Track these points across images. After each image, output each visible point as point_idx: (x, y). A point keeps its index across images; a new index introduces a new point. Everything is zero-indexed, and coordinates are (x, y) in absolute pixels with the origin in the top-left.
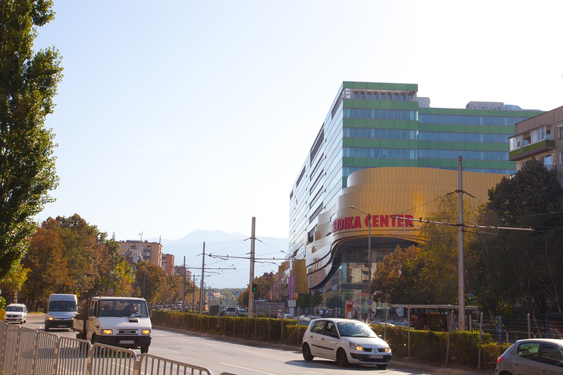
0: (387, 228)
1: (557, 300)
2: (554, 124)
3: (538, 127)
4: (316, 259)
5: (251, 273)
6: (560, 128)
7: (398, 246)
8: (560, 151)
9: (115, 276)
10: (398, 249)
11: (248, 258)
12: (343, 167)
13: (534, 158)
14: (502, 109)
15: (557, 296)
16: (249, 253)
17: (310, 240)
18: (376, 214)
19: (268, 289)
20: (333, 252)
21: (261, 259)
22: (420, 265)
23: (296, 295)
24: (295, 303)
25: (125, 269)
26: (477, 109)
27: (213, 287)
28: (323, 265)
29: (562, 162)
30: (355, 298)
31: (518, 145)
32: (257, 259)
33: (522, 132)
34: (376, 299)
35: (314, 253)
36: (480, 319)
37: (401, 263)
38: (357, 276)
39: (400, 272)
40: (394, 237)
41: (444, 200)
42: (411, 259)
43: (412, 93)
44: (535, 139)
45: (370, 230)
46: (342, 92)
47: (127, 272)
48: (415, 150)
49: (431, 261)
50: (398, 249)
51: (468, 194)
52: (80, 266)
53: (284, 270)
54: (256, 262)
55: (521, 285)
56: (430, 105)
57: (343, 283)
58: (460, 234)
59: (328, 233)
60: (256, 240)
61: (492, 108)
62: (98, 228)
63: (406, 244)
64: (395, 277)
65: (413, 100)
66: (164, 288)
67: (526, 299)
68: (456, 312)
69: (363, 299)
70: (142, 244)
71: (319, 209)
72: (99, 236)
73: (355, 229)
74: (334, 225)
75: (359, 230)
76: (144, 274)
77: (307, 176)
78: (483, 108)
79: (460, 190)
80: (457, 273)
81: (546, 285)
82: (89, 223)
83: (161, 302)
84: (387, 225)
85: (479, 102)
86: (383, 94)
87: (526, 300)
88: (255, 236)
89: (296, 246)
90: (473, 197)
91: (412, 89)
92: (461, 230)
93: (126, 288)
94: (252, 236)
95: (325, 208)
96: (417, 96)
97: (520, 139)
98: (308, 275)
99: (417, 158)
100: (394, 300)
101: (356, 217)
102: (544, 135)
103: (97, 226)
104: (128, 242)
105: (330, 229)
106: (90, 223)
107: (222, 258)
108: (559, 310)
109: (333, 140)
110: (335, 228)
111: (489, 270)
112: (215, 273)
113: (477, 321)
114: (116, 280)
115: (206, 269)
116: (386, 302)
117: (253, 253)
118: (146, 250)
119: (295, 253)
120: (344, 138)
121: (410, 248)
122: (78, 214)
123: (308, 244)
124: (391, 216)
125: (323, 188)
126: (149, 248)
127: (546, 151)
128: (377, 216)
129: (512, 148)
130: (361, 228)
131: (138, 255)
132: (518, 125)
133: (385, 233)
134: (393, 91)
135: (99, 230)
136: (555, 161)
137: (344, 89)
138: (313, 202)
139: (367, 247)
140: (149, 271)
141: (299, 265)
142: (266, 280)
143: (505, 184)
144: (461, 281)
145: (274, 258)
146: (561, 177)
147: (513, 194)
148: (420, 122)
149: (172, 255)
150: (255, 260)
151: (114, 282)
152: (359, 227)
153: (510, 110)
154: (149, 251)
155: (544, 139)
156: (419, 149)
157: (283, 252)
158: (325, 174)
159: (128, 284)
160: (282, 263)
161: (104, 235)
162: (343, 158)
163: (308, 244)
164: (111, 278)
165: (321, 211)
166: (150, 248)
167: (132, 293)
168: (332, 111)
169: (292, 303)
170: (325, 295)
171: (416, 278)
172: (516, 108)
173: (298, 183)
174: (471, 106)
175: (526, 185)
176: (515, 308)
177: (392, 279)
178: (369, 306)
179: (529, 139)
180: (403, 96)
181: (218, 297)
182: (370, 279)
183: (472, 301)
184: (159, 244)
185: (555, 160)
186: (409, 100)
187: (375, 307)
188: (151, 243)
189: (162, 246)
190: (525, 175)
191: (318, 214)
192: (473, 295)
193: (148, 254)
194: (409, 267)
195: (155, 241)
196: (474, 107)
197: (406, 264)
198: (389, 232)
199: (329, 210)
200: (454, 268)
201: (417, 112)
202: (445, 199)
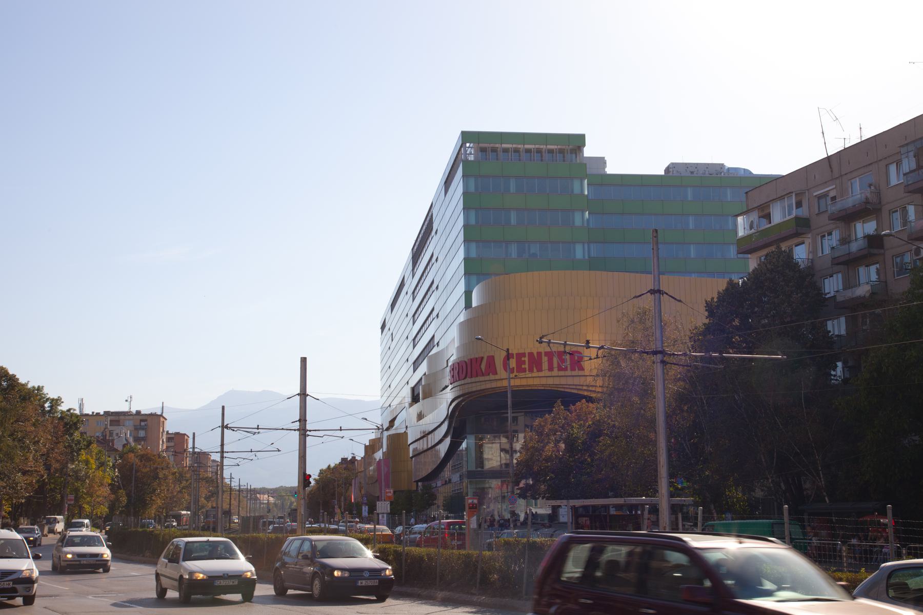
0: (541, 374)
1: (823, 483)
2: (808, 190)
3: (782, 196)
4: (424, 432)
5: (301, 455)
6: (818, 197)
7: (559, 401)
8: (818, 235)
9: (76, 472)
10: (559, 407)
11: (295, 430)
12: (465, 274)
13: (779, 247)
14: (723, 174)
15: (822, 476)
16: (296, 421)
17: (415, 399)
18: (521, 351)
19: (348, 485)
20: (450, 417)
21: (319, 430)
22: (595, 433)
23: (390, 492)
24: (389, 506)
25: (98, 459)
26: (682, 175)
27: (256, 485)
28: (437, 441)
29: (822, 253)
30: (491, 494)
31: (751, 227)
32: (310, 431)
33: (756, 205)
34: (523, 495)
35: (421, 421)
36: (696, 518)
37: (564, 430)
38: (493, 456)
39: (563, 446)
40: (553, 389)
41: (633, 321)
42: (579, 423)
43: (576, 150)
44: (777, 217)
45: (510, 378)
46: (460, 150)
47: (102, 465)
48: (583, 243)
49: (614, 426)
50: (559, 407)
51: (671, 296)
52: (9, 458)
53: (374, 453)
54: (308, 435)
55: (763, 460)
56: (606, 170)
57: (468, 470)
58: (658, 369)
59: (443, 386)
60: (308, 398)
61: (707, 172)
62: (45, 391)
63: (570, 399)
64: (554, 456)
65: (578, 161)
66: (168, 490)
67: (771, 482)
68: (655, 510)
69: (503, 495)
70: (131, 417)
71: (428, 347)
72: (47, 405)
73: (487, 378)
74: (452, 372)
75: (493, 379)
76: (133, 468)
77: (407, 293)
78: (692, 173)
79: (656, 289)
80: (654, 443)
81: (804, 458)
82: (28, 382)
83: (165, 514)
84: (540, 369)
85: (686, 164)
86: (528, 151)
87: (771, 485)
88: (306, 390)
89: (393, 410)
90: (680, 301)
91: (577, 142)
92: (659, 361)
93: (99, 493)
94: (300, 391)
95: (438, 346)
96: (585, 156)
97: (754, 216)
98: (412, 458)
99: (587, 257)
100: (554, 494)
101: (489, 357)
102: (793, 210)
103: (43, 387)
104: (107, 413)
105: (447, 379)
106: (29, 383)
107: (247, 430)
108: (827, 499)
109: (448, 230)
110: (453, 376)
111: (709, 437)
112: (244, 459)
113: (692, 524)
114: (78, 479)
115: (227, 452)
116: (541, 498)
117: (303, 420)
118: (139, 427)
119: (392, 422)
120: (466, 227)
121: (578, 404)
122: (4, 367)
123: (411, 405)
125: (433, 312)
126: (143, 424)
127: (797, 235)
128: (523, 355)
129: (741, 233)
130: (496, 376)
131: (125, 434)
132: (749, 193)
133: (536, 382)
134: (545, 146)
135: (47, 394)
136: (811, 252)
137: (464, 145)
138: (418, 336)
139: (506, 407)
140: (141, 461)
141: (398, 441)
142: (345, 470)
143: (733, 291)
144: (662, 453)
145: (341, 427)
146: (821, 278)
147: (746, 307)
148: (591, 198)
149: (185, 434)
150: (308, 433)
151: (76, 484)
152: (493, 374)
153: (735, 175)
154: (142, 428)
155: (793, 216)
156: (589, 242)
157: (366, 419)
158: (437, 288)
159: (102, 484)
160: (370, 440)
161: (56, 402)
162: (465, 259)
163: (411, 405)
164: (70, 476)
165: (431, 350)
166: (146, 423)
167: (110, 500)
168: (445, 182)
169: (383, 507)
170: (443, 492)
171: (590, 456)
172: (744, 172)
173: (393, 305)
174: (673, 171)
175: (766, 292)
176: (753, 499)
177: (548, 459)
178: (511, 506)
179: (768, 217)
180: (561, 155)
181: (264, 502)
182: (512, 460)
183: (683, 491)
184: (161, 415)
185: (810, 250)
186: (571, 161)
187: (522, 508)
188: (146, 415)
189: (166, 419)
190: (765, 274)
191: (428, 355)
192: (684, 481)
193: (142, 434)
194: (576, 437)
195: (153, 412)
196: (678, 172)
197: (572, 432)
198: (544, 381)
199: (444, 349)
200: (652, 436)
201: (586, 181)
202: (635, 318)
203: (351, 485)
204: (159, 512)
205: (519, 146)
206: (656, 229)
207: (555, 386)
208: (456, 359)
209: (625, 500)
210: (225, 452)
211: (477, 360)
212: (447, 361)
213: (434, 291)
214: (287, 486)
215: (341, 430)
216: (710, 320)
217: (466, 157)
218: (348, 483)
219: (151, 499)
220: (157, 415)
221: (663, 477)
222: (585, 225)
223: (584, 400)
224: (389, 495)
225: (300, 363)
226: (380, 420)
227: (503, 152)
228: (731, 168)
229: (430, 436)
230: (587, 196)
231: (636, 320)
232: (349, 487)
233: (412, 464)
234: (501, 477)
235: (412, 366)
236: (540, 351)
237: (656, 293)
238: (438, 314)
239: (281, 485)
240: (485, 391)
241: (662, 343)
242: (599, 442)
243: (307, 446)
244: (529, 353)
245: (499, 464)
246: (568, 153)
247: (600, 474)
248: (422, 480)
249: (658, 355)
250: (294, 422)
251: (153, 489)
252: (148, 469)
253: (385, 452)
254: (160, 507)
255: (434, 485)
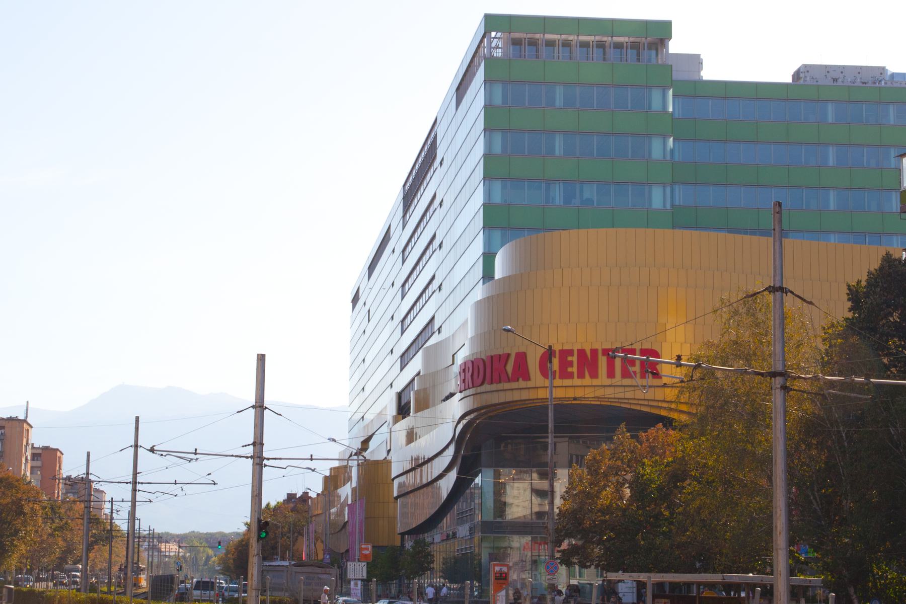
0: (595, 382)
4: (417, 459)
5: (255, 494)
7: (623, 425)
10: (622, 435)
11: (247, 457)
14: (883, 82)
16: (249, 445)
17: (403, 410)
20: (459, 441)
21: (281, 459)
24: (365, 569)
30: (514, 558)
32: (268, 459)
34: (566, 560)
35: (412, 444)
39: (627, 492)
41: (736, 312)
42: (653, 459)
45: (552, 387)
46: (481, 41)
48: (664, 185)
50: (622, 435)
53: (337, 487)
56: (702, 73)
57: (482, 520)
58: (778, 397)
59: (447, 394)
60: (266, 412)
64: (614, 505)
65: (660, 62)
66: (36, 532)
71: (423, 334)
73: (514, 385)
74: (463, 375)
77: (393, 251)
78: (835, 80)
79: (777, 285)
80: (769, 496)
83: (29, 567)
84: (594, 375)
85: (826, 66)
86: (585, 45)
89: (368, 425)
92: (779, 386)
94: (256, 402)
95: (439, 333)
96: (670, 51)
98: (396, 498)
99: (668, 207)
100: (611, 563)
105: (453, 384)
107: (180, 455)
110: (464, 381)
115: (142, 483)
116: (593, 567)
117: (258, 443)
119: (365, 443)
120: (488, 157)
121: (652, 431)
123: (396, 420)
124: (605, 352)
125: (434, 282)
128: (570, 352)
133: (589, 393)
134: (610, 38)
137: (487, 34)
138: (409, 316)
139: (545, 429)
142: (292, 511)
149: (57, 450)
156: (674, 183)
157: (334, 440)
158: (440, 246)
163: (396, 420)
168: (458, 89)
178: (550, 577)
180: (635, 52)
182: (553, 509)
183: (807, 565)
184: (25, 421)
186: (650, 60)
189: (31, 427)
194: (648, 480)
195: (14, 415)
196: (813, 78)
197: (642, 472)
198: (600, 393)
199: (449, 337)
200: (763, 482)
201: (671, 92)
202: (740, 309)
203: (301, 534)
204: (21, 563)
205: (571, 38)
206: (779, 202)
207: (617, 400)
208: (469, 355)
209: (723, 576)
210: (139, 483)
211: (500, 358)
212: (453, 356)
213: (435, 250)
214: (201, 532)
215: (312, 459)
216: (854, 314)
217: (491, 53)
218: (297, 531)
219: (12, 544)
220: (20, 420)
221: (780, 549)
222: (668, 158)
223: (661, 424)
224: (366, 552)
225: (256, 362)
226: (349, 441)
227: (546, 45)
228: (896, 73)
229: (424, 468)
230: (672, 114)
231: (741, 311)
232: (297, 537)
233: (395, 508)
234: (530, 533)
235: (400, 359)
236: (594, 347)
237: (777, 291)
238: (441, 284)
239: (192, 530)
240: (511, 404)
241: (784, 360)
242: (683, 488)
243: (263, 480)
244: (579, 351)
245: (528, 512)
246: (644, 49)
247: (683, 536)
248: (409, 533)
249: (777, 378)
250: (246, 446)
251: (15, 530)
252: (9, 500)
253: (356, 487)
254: (22, 556)
255: (429, 540)
